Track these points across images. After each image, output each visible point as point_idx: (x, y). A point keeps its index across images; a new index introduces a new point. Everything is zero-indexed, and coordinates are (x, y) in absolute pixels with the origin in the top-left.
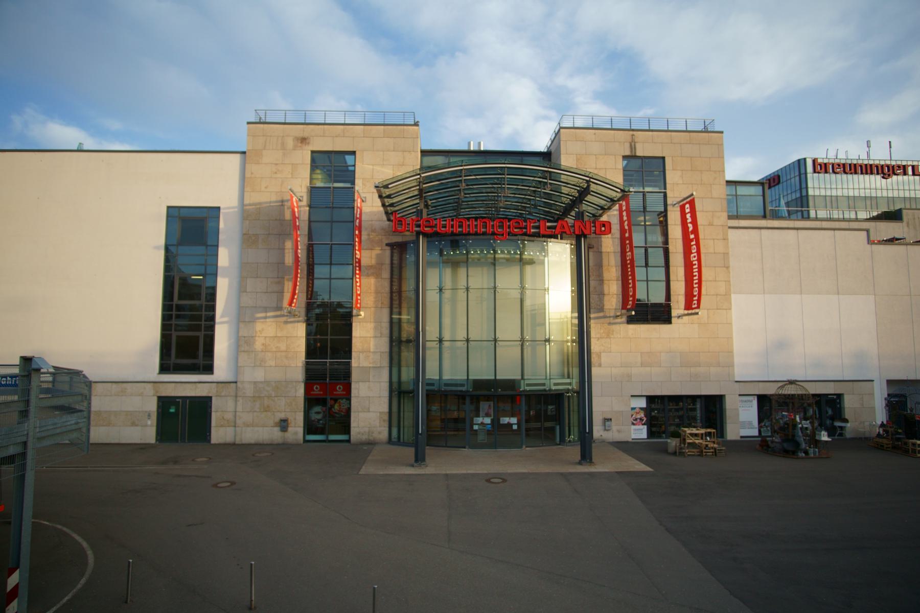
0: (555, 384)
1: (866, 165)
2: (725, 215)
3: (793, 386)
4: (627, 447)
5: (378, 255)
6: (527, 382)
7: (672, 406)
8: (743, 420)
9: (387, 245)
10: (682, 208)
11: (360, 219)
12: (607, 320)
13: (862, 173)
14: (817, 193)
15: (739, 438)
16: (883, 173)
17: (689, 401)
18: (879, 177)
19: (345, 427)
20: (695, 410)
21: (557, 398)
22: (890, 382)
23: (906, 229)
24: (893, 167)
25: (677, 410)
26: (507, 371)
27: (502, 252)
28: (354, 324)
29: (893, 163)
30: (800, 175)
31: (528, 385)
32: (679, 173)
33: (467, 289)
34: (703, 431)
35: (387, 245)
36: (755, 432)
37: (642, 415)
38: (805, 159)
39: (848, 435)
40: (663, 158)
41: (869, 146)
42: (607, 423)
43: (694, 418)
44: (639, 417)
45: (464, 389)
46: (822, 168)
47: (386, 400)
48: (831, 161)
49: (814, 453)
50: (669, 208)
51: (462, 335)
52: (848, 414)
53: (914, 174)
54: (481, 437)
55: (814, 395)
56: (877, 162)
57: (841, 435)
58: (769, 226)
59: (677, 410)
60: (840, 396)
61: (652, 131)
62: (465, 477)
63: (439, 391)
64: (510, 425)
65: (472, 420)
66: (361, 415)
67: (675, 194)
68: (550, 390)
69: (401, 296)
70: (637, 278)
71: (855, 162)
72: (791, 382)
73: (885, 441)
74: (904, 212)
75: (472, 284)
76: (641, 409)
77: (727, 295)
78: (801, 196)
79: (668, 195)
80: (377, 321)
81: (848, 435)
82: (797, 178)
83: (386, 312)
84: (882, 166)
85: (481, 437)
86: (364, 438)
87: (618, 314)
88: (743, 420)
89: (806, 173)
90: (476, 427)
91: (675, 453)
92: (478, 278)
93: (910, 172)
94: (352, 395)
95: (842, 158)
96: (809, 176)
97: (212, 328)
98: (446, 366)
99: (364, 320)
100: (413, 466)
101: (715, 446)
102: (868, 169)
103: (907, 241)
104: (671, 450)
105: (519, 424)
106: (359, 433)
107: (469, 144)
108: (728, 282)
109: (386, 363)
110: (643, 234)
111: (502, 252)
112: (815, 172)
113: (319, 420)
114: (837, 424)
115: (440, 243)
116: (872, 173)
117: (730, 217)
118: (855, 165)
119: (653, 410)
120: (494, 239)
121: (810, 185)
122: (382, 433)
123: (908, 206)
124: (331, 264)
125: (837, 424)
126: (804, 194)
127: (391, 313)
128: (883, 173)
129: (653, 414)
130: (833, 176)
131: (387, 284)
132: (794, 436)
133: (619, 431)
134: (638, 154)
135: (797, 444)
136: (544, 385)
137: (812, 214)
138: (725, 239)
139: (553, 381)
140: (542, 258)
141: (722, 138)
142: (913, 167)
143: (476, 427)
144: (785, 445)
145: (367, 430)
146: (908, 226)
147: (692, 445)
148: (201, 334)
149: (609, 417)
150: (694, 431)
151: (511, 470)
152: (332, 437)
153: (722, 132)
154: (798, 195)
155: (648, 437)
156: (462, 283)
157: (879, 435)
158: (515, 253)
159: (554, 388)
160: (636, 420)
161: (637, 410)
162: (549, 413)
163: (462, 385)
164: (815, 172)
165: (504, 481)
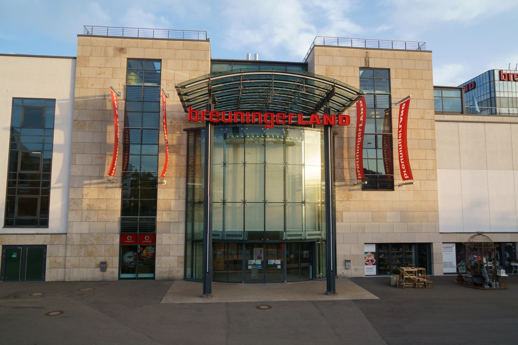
0: (309, 235)
2: (433, 111)
6: (288, 233)
7: (394, 251)
8: (445, 261)
9: (184, 130)
10: (401, 105)
12: (348, 188)
14: (502, 95)
15: (443, 275)
20: (410, 254)
25: (398, 254)
26: (274, 225)
27: (251, 136)
28: (158, 190)
30: (490, 82)
31: (289, 235)
32: (400, 81)
34: (416, 269)
35: (184, 130)
37: (373, 257)
38: (493, 70)
44: (370, 259)
46: (505, 77)
47: (183, 247)
48: (513, 72)
49: (496, 285)
50: (393, 106)
55: (495, 243)
58: (466, 120)
61: (381, 49)
63: (222, 240)
64: (275, 265)
67: (397, 96)
68: (305, 239)
72: (479, 234)
77: (434, 170)
78: (491, 98)
79: (392, 97)
80: (177, 188)
83: (183, 180)
85: (254, 275)
86: (165, 276)
88: (445, 261)
89: (494, 81)
90: (250, 267)
91: (395, 286)
92: (252, 156)
97: (47, 192)
98: (229, 221)
99: (166, 187)
100: (202, 297)
101: (425, 280)
105: (282, 264)
106: (162, 272)
107: (248, 55)
109: (183, 219)
111: (271, 137)
112: (500, 80)
115: (224, 130)
117: (437, 113)
121: (497, 89)
126: (493, 96)
127: (187, 181)
129: (381, 257)
130: (514, 83)
131: (184, 160)
132: (481, 273)
133: (356, 270)
134: (370, 66)
135: (484, 279)
136: (301, 235)
138: (433, 129)
139: (307, 233)
140: (300, 141)
143: (250, 267)
144: (475, 279)
145: (167, 269)
148: (39, 197)
149: (348, 259)
150: (410, 269)
152: (141, 275)
153: (431, 52)
154: (489, 97)
155: (377, 274)
156: (241, 159)
158: (280, 137)
159: (308, 238)
160: (368, 261)
162: (304, 257)
163: (240, 236)
164: (500, 80)
165: (270, 307)
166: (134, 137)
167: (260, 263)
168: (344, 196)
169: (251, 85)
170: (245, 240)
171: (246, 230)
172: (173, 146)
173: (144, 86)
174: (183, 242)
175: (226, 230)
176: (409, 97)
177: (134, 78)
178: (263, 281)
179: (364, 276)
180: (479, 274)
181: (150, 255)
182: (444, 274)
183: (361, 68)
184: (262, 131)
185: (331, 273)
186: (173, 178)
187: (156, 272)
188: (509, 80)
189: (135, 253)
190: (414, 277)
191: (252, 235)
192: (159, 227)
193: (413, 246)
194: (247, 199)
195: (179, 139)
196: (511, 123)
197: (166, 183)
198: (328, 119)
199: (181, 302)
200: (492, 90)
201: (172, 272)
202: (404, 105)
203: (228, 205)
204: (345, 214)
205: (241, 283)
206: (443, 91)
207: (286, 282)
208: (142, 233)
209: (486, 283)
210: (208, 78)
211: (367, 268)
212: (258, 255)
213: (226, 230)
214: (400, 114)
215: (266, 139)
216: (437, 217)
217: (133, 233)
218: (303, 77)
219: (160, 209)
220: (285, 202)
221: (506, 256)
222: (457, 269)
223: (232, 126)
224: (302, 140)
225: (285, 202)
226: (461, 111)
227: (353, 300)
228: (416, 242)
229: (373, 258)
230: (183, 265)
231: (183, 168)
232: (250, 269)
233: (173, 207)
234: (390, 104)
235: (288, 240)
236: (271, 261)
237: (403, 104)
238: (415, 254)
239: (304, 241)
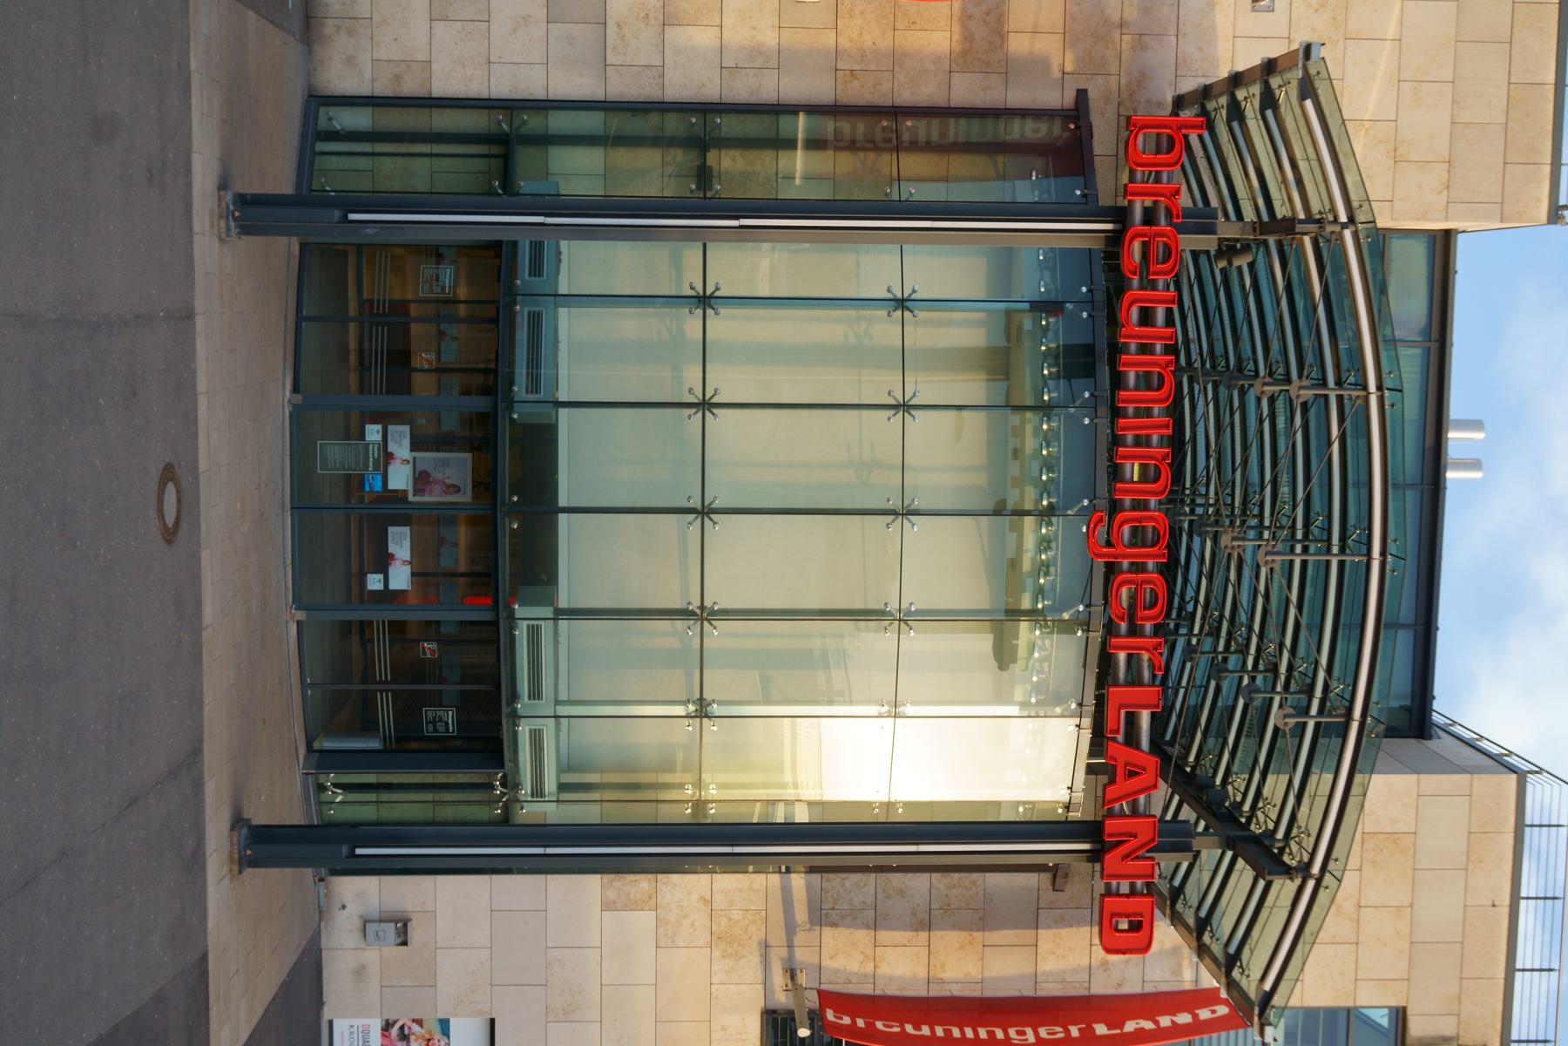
0: (536, 737)
6: (546, 628)
9: (1082, 95)
12: (778, 936)
21: (484, 739)
26: (590, 559)
31: (534, 634)
35: (1082, 95)
42: (390, 929)
45: (520, 389)
47: (476, 88)
51: (728, 382)
54: (334, 454)
62: (184, 389)
63: (512, 294)
64: (383, 562)
68: (515, 717)
80: (780, 60)
83: (821, 89)
85: (334, 454)
87: (802, 979)
90: (373, 433)
98: (608, 326)
100: (223, 186)
105: (388, 596)
107: (1476, 425)
109: (621, 87)
111: (1044, 544)
120: (1093, 509)
127: (814, 110)
133: (360, 972)
136: (536, 693)
140: (1019, 695)
143: (373, 433)
149: (415, 934)
156: (926, 388)
158: (1040, 592)
159: (524, 730)
165: (170, 535)
167: (393, 586)
168: (736, 915)
169: (1316, 439)
170: (510, 408)
174: (502, 87)
175: (563, 313)
183: (1400, 1016)
186: (829, 39)
191: (539, 445)
194: (721, 422)
195: (1037, 65)
199: (196, 80)
204: (646, 918)
205: (295, 390)
210: (1351, 220)
211: (366, 1031)
218: (1372, 387)
220: (703, 615)
223: (1102, 346)
224: (1024, 704)
225: (703, 615)
230: (383, 88)
231: (886, 87)
232: (362, 435)
233: (676, 36)
235: (512, 628)
236: (407, 544)
239: (505, 710)
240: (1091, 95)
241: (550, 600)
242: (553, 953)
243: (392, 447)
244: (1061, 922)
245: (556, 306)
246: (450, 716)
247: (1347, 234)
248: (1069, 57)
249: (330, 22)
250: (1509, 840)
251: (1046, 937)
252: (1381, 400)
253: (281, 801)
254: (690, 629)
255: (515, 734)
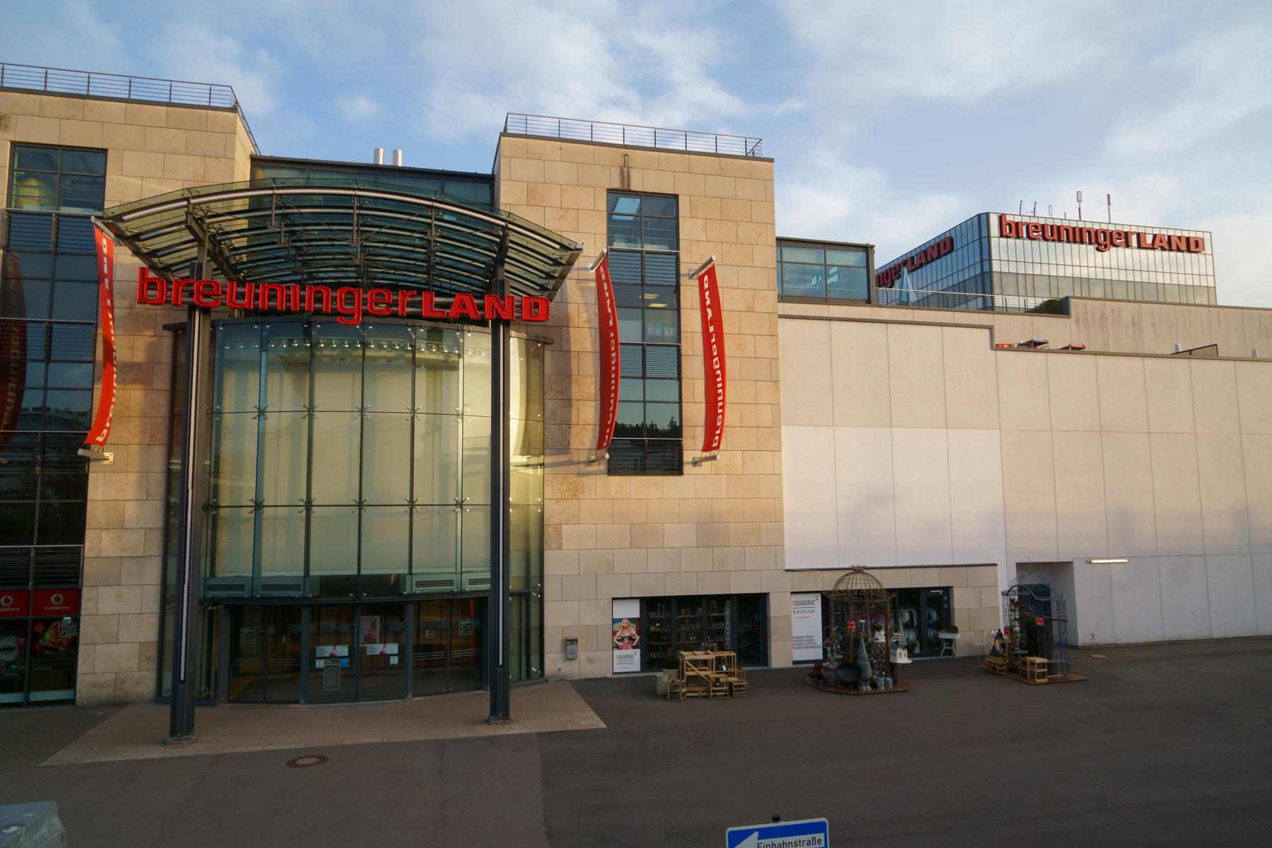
0: (472, 582)
1: (1074, 229)
2: (774, 295)
3: (859, 576)
4: (593, 690)
5: (150, 345)
6: (415, 579)
7: (685, 614)
8: (798, 634)
9: (165, 327)
10: (701, 279)
11: (110, 275)
12: (574, 468)
13: (1068, 241)
14: (1005, 269)
15: (791, 665)
16: (1097, 242)
17: (714, 602)
18: (1092, 248)
19: (67, 675)
20: (722, 619)
21: (477, 606)
22: (1021, 567)
23: (1074, 328)
24: (1111, 233)
25: (693, 621)
26: (384, 558)
27: (328, 344)
28: (91, 476)
29: (1111, 228)
30: (980, 239)
31: (419, 584)
32: (701, 223)
33: (261, 412)
34: (711, 656)
35: (165, 327)
36: (817, 654)
37: (633, 631)
38: (987, 214)
39: (959, 653)
40: (676, 196)
41: (1079, 201)
42: (570, 647)
43: (721, 632)
44: (627, 634)
45: (297, 594)
46: (1012, 229)
47: (154, 620)
48: (1026, 220)
49: (886, 684)
50: (683, 280)
51: (248, 496)
52: (959, 619)
53: (1139, 247)
54: (330, 683)
55: (890, 591)
56: (1089, 226)
57: (949, 652)
58: (875, 317)
59: (693, 621)
60: (947, 590)
61: (659, 150)
62: (254, 757)
63: (252, 599)
64: (385, 657)
65: (314, 651)
66: (100, 649)
67: (690, 260)
68: (462, 592)
69: (182, 427)
70: (29, 382)
71: (1058, 223)
72: (857, 570)
73: (1000, 661)
74: (1072, 301)
75: (272, 403)
76: (630, 620)
77: (775, 427)
78: (983, 273)
79: (682, 259)
80: (144, 472)
81: (959, 653)
82: (977, 243)
83: (159, 452)
84: (1096, 232)
85: (330, 682)
86: (105, 693)
87: (593, 458)
88: (798, 634)
89: (989, 237)
90: (320, 664)
91: (664, 696)
92: (335, 392)
93: (1134, 243)
94: (83, 612)
95: (1043, 215)
96: (994, 241)
98: (274, 555)
99: (114, 468)
100: (164, 743)
101: (732, 679)
102: (1076, 235)
103: (1052, 346)
104: (660, 690)
105: (401, 654)
106: (94, 685)
107: (377, 152)
108: (776, 405)
109: (155, 548)
110: (639, 324)
111: (380, 347)
112: (1002, 236)
113: (9, 664)
114: (944, 635)
115: (263, 329)
116: (1082, 242)
117: (782, 298)
118: (1059, 227)
119: (653, 622)
120: (413, 327)
121: (995, 255)
122: (144, 681)
123: (1078, 294)
124: (644, 377)
125: (944, 635)
126: (986, 269)
127: (170, 455)
128: (1097, 242)
129: (652, 628)
130: (1028, 242)
132: (856, 658)
133: (590, 661)
134: (633, 188)
135: (859, 670)
136: (451, 583)
137: (999, 301)
138: (773, 335)
139: (466, 577)
140: (455, 359)
141: (771, 171)
142: (1138, 235)
143: (320, 664)
144: (840, 673)
145: (111, 677)
146: (1087, 328)
147: (696, 680)
149: (573, 636)
150: (700, 655)
151: (461, 735)
152: (36, 696)
153: (772, 160)
154: (978, 271)
155: (643, 670)
156: (252, 401)
157: (994, 652)
158: (403, 348)
159: (468, 588)
160: (622, 639)
161: (625, 623)
162: (467, 634)
163: (296, 587)
164: (1002, 236)
165: (323, 760)
166: (628, 361)
167: (396, 652)
168: (564, 488)
169: (378, 222)
170: (307, 598)
171: (312, 573)
172: (133, 366)
173: (58, 215)
174: (154, 607)
175: (264, 574)
176: (711, 260)
177: (36, 193)
178: (355, 696)
179: (610, 675)
180: (851, 661)
181: (64, 643)
182: (795, 663)
184: (408, 336)
185: (499, 670)
186: (134, 449)
187: (78, 686)
188: (1018, 237)
189: (22, 640)
190: (708, 673)
191: (332, 585)
192: (90, 569)
193: (728, 603)
195: (151, 349)
196: (886, 322)
197: (111, 458)
198: (497, 305)
199: (97, 760)
200: (986, 256)
201: (124, 682)
202: (706, 278)
203: (267, 512)
204: (566, 529)
205: (298, 702)
206: (828, 253)
207: (410, 695)
208: (42, 587)
209: (865, 680)
210: (187, 199)
211: (620, 657)
212: (367, 632)
213: (264, 574)
214: (703, 300)
215: (417, 356)
216: (781, 532)
217: (16, 587)
218: (270, 192)
219: (94, 525)
220: (412, 504)
221: (930, 618)
222: (825, 652)
223: (430, 324)
224: (459, 356)
225: (412, 504)
226: (866, 297)
227: (540, 734)
228: (733, 592)
229: (633, 632)
230: (153, 666)
231: (159, 421)
232: (321, 670)
233: (130, 521)
234: (678, 275)
235: (416, 595)
236: (325, 648)
237: (703, 276)
238: (732, 620)
239: (458, 597)
240: (165, 322)
241: (404, 576)
242: (582, 572)
243: (327, 655)
244: (568, 341)
245: (260, 577)
246: (464, 623)
247: (193, 201)
248: (146, 333)
249: (118, 693)
250: (531, 141)
251: (574, 347)
252: (278, 188)
253: (481, 700)
254: (316, 511)
255: (420, 595)
